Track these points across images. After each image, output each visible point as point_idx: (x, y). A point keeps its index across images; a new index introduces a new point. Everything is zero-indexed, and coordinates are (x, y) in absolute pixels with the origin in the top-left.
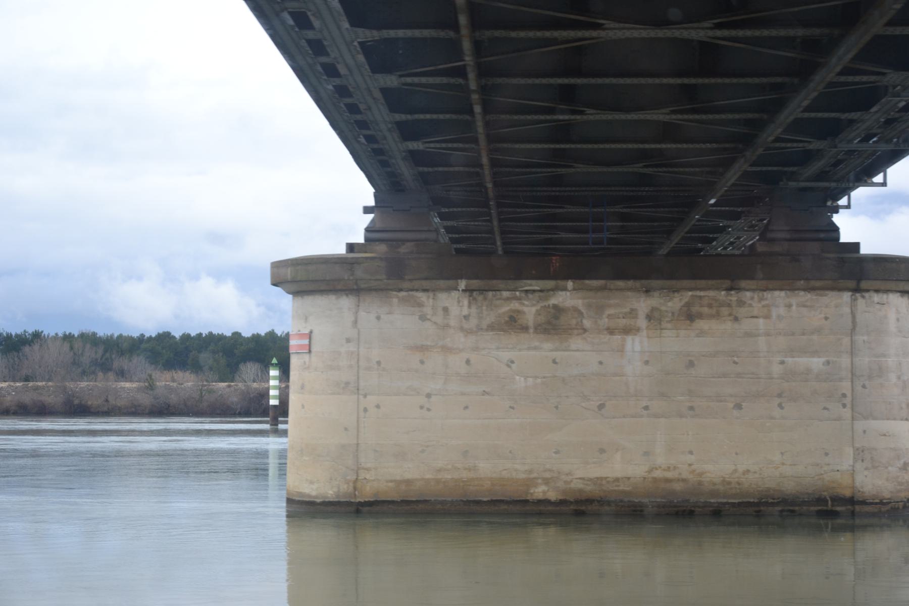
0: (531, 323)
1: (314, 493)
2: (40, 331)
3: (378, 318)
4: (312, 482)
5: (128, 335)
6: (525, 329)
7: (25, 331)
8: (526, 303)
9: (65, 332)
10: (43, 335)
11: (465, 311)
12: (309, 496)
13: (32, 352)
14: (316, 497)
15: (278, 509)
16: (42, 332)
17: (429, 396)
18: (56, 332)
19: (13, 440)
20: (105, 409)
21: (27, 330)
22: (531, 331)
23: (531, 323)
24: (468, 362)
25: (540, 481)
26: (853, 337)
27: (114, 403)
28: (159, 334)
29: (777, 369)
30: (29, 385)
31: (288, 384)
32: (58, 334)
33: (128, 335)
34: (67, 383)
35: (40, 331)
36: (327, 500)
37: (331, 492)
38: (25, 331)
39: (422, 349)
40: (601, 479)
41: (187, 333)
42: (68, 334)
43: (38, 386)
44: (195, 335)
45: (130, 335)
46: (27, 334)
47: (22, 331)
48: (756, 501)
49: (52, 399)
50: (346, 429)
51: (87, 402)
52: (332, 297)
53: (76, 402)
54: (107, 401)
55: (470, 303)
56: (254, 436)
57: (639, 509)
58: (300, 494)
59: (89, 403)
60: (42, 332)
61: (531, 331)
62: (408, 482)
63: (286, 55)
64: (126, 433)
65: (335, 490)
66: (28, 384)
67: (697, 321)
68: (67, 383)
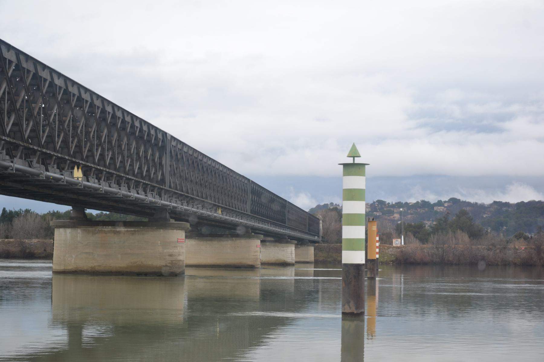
2: (29, 209)
5: (89, 213)
7: (20, 210)
9: (54, 210)
10: (31, 211)
13: (17, 223)
16: (30, 210)
18: (49, 210)
20: (43, 255)
21: (22, 209)
27: (50, 251)
28: (509, 203)
29: (453, 246)
30: (5, 241)
31: (48, 241)
32: (51, 211)
33: (89, 213)
35: (29, 209)
38: (20, 210)
41: (43, 214)
42: (56, 212)
43: (10, 241)
44: (309, 210)
45: (90, 213)
46: (21, 211)
47: (19, 209)
49: (13, 249)
51: (34, 251)
53: (28, 251)
54: (45, 250)
56: (9, 266)
59: (36, 251)
60: (30, 210)
64: (12, 269)
66: (5, 240)
67: (13, 219)
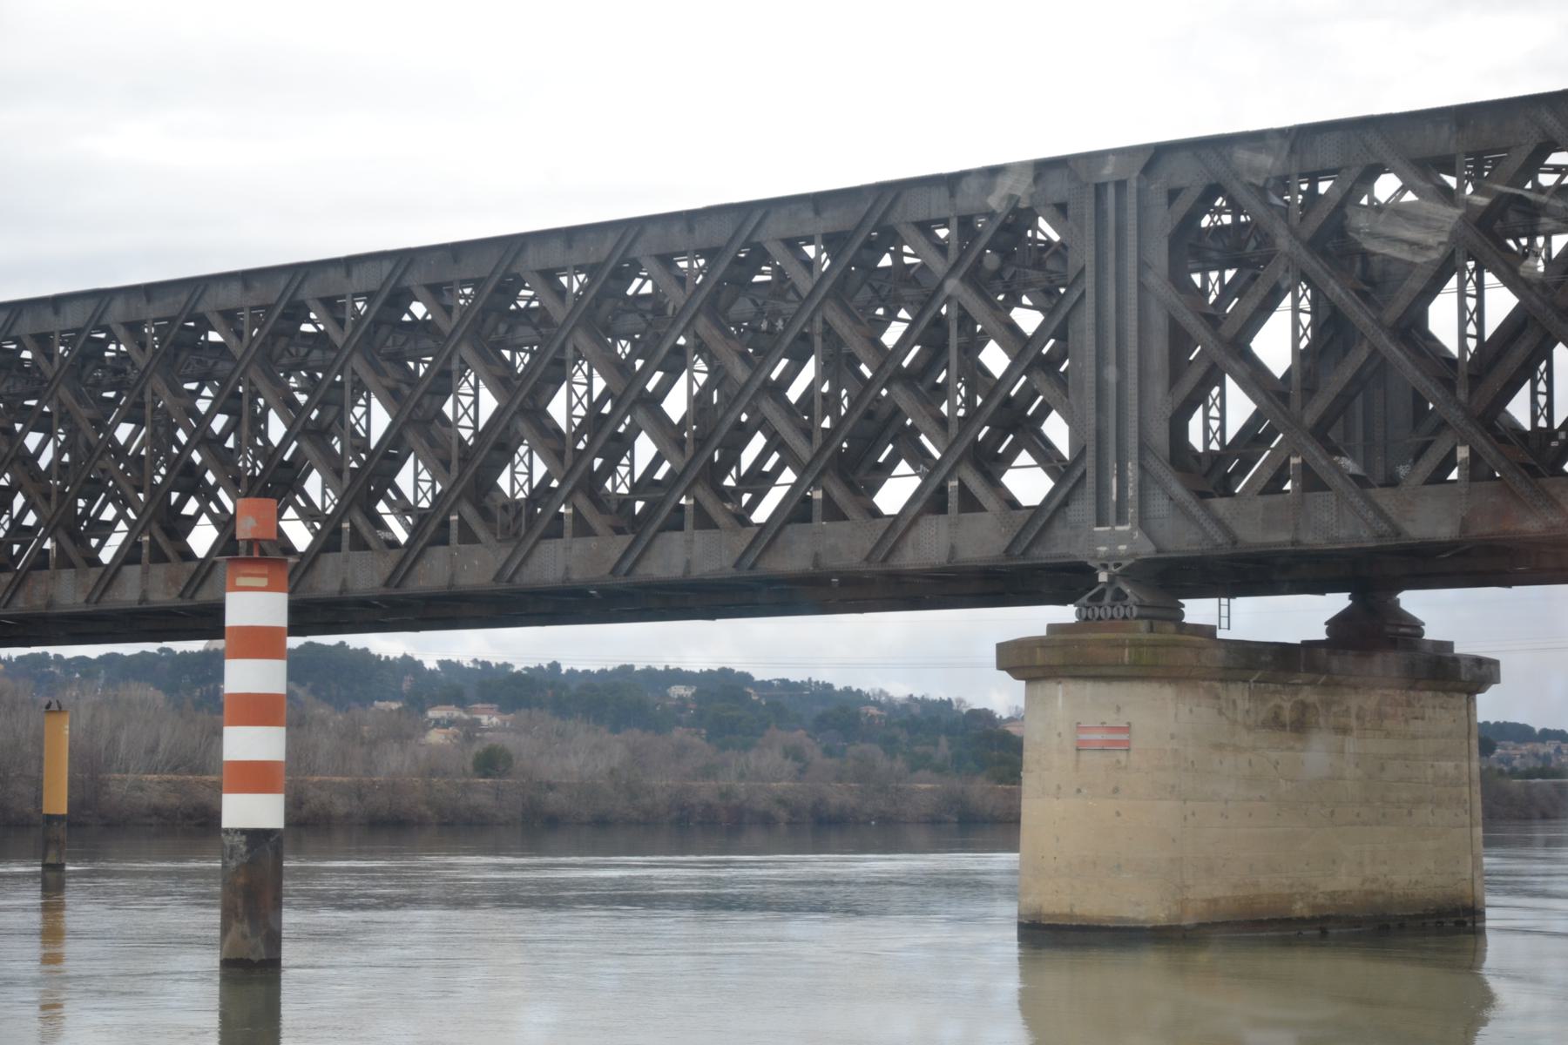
0: (1288, 722)
1: (1142, 917)
3: (1191, 711)
4: (1138, 904)
6: (1283, 726)
8: (1285, 697)
11: (1247, 707)
12: (1134, 920)
14: (1144, 921)
15: (1004, 944)
17: (1226, 802)
19: (996, 857)
22: (1288, 728)
23: (1288, 722)
24: (1250, 763)
25: (1297, 896)
26: (1306, 687)
34: (103, 672)
36: (1159, 924)
37: (1162, 915)
39: (1219, 747)
40: (1334, 892)
48: (1421, 912)
50: (1174, 840)
52: (1155, 686)
55: (1250, 696)
57: (47, 945)
58: (1121, 919)
61: (1288, 728)
62: (1215, 901)
63: (1191, 449)
65: (1167, 912)
68: (103, 672)
